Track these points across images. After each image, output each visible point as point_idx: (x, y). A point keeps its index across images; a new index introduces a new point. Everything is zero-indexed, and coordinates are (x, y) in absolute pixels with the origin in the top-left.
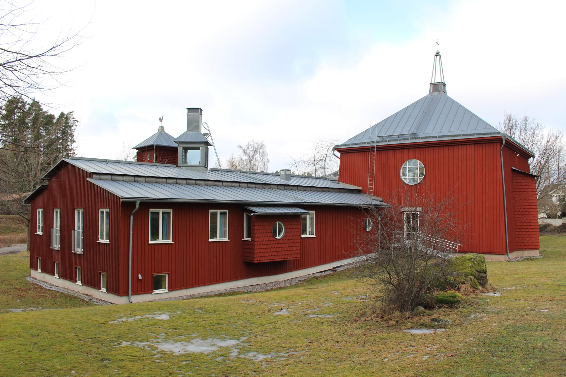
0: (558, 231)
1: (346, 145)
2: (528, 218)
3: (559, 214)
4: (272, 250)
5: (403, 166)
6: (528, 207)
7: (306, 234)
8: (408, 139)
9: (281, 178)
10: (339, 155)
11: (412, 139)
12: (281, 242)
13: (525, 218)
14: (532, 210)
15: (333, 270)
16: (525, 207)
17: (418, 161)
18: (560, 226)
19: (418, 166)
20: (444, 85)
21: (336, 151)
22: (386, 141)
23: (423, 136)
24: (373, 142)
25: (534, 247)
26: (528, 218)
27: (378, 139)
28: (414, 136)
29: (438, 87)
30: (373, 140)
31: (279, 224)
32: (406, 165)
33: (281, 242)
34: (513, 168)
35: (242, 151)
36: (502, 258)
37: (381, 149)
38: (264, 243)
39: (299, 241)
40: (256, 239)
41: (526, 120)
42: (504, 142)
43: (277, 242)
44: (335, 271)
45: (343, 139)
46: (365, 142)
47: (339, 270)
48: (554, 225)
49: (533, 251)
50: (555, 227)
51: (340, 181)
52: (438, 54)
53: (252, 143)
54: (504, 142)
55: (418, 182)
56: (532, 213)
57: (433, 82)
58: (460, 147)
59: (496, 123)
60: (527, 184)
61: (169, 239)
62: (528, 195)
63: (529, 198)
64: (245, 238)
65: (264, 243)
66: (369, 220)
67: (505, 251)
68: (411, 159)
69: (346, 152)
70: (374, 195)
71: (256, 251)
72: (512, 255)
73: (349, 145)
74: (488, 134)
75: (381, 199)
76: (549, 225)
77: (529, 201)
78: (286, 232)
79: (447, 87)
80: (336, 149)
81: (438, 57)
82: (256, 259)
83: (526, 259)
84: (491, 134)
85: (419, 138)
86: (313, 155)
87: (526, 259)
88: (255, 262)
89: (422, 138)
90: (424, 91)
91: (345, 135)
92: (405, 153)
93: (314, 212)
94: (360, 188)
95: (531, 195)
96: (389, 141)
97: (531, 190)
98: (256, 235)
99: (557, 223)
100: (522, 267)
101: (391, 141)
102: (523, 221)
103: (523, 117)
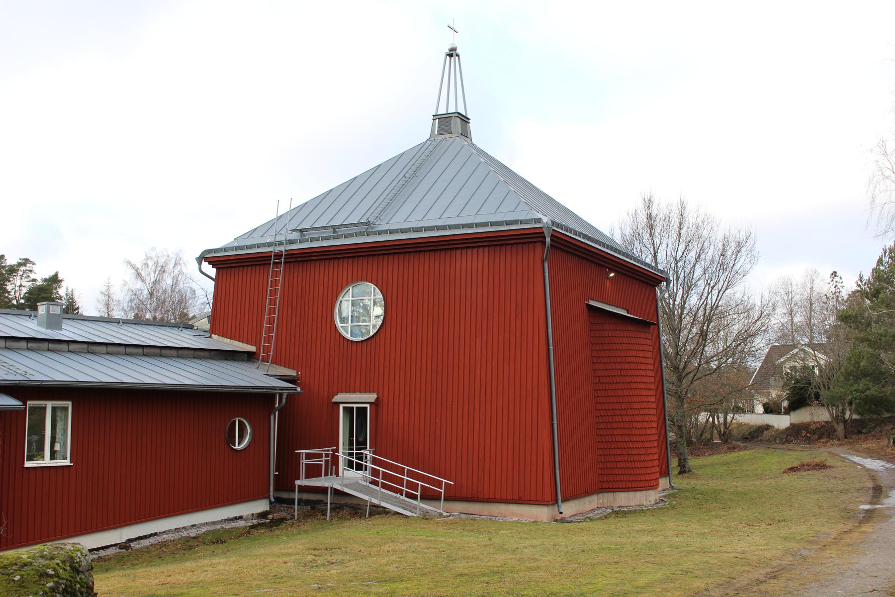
0: (781, 439)
1: (231, 249)
2: (627, 419)
3: (785, 404)
6: (626, 392)
7: (43, 457)
8: (351, 236)
9: (40, 324)
11: (361, 234)
13: (619, 419)
14: (635, 399)
15: (125, 546)
16: (620, 393)
17: (373, 286)
18: (787, 429)
20: (465, 120)
25: (647, 484)
26: (627, 419)
27: (295, 236)
28: (367, 226)
29: (452, 124)
30: (286, 239)
31: (240, 421)
34: (592, 303)
35: (131, 271)
36: (543, 513)
37: (298, 259)
41: (682, 205)
42: (548, 240)
45: (224, 236)
46: (267, 242)
48: (776, 426)
49: (638, 493)
50: (777, 430)
51: (213, 330)
53: (153, 254)
54: (548, 240)
55: (372, 334)
56: (636, 406)
57: (442, 111)
58: (459, 252)
59: (605, 213)
60: (625, 340)
62: (627, 366)
63: (630, 373)
67: (548, 496)
68: (357, 280)
69: (228, 265)
70: (275, 362)
72: (569, 509)
74: (515, 222)
75: (292, 373)
76: (768, 427)
77: (628, 379)
79: (472, 126)
80: (206, 259)
83: (619, 513)
84: (521, 222)
85: (380, 233)
87: (619, 513)
89: (385, 232)
90: (421, 131)
93: (69, 404)
94: (252, 349)
95: (633, 366)
96: (312, 240)
97: (634, 353)
99: (781, 422)
100: (594, 536)
101: (317, 239)
102: (614, 425)
103: (675, 202)
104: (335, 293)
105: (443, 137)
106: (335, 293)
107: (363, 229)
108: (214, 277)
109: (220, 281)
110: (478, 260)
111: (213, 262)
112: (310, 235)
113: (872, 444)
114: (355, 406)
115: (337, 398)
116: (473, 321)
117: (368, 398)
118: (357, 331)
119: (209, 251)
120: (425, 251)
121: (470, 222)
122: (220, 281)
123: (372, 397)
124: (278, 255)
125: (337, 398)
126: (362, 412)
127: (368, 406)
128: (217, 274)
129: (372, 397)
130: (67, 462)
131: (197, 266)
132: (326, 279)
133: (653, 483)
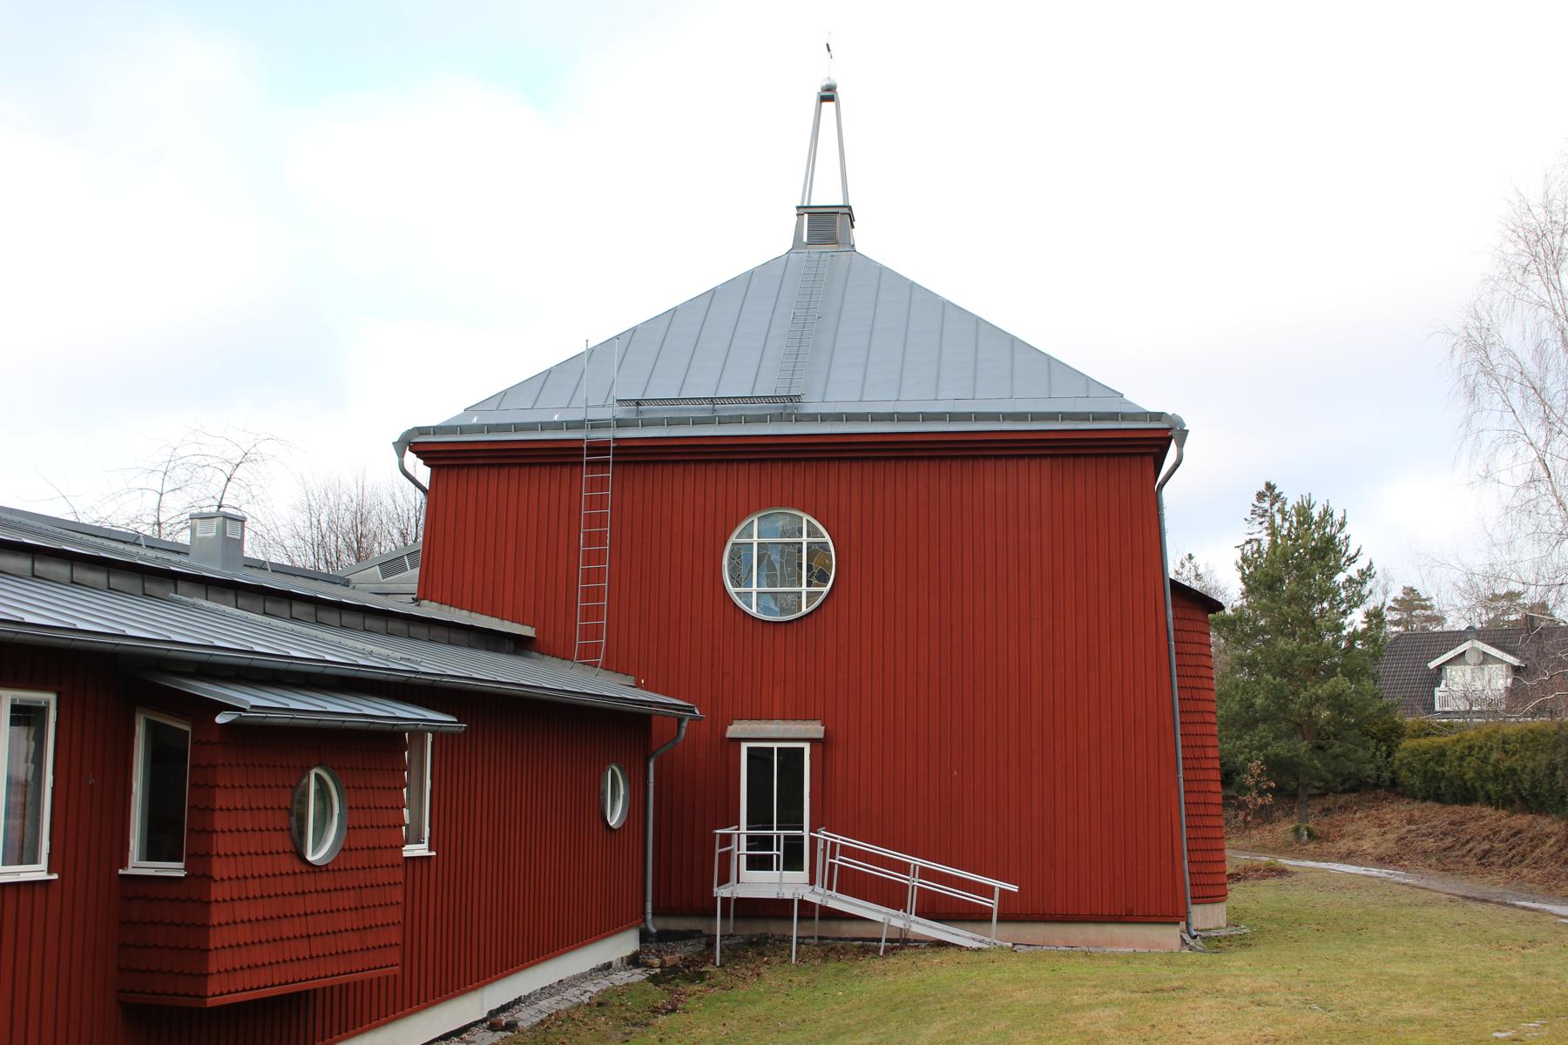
1: (463, 430)
4: (288, 929)
5: (733, 539)
8: (760, 419)
10: (423, 473)
12: (325, 881)
15: (492, 1022)
19: (805, 539)
21: (410, 458)
22: (658, 423)
24: (595, 425)
27: (621, 412)
28: (787, 406)
29: (826, 225)
30: (590, 409)
33: (325, 881)
38: (254, 887)
39: (399, 875)
40: (219, 868)
43: (309, 883)
44: (511, 1026)
45: (444, 404)
46: (557, 414)
47: (527, 1018)
49: (1209, 906)
55: (804, 610)
64: (137, 865)
65: (254, 887)
66: (613, 773)
69: (457, 462)
71: (216, 938)
73: (479, 429)
78: (349, 828)
81: (828, 107)
82: (213, 986)
85: (813, 418)
86: (151, 500)
88: (212, 1002)
90: (775, 235)
91: (458, 387)
94: (528, 631)
96: (672, 422)
98: (221, 844)
107: (774, 408)
108: (426, 484)
110: (1034, 478)
111: (427, 453)
112: (652, 412)
114: (775, 745)
115: (735, 730)
117: (801, 732)
120: (675, 462)
121: (1018, 410)
124: (598, 448)
125: (735, 730)
127: (807, 747)
128: (434, 479)
129: (816, 729)
130: (37, 872)
131: (396, 459)
133: (1218, 891)
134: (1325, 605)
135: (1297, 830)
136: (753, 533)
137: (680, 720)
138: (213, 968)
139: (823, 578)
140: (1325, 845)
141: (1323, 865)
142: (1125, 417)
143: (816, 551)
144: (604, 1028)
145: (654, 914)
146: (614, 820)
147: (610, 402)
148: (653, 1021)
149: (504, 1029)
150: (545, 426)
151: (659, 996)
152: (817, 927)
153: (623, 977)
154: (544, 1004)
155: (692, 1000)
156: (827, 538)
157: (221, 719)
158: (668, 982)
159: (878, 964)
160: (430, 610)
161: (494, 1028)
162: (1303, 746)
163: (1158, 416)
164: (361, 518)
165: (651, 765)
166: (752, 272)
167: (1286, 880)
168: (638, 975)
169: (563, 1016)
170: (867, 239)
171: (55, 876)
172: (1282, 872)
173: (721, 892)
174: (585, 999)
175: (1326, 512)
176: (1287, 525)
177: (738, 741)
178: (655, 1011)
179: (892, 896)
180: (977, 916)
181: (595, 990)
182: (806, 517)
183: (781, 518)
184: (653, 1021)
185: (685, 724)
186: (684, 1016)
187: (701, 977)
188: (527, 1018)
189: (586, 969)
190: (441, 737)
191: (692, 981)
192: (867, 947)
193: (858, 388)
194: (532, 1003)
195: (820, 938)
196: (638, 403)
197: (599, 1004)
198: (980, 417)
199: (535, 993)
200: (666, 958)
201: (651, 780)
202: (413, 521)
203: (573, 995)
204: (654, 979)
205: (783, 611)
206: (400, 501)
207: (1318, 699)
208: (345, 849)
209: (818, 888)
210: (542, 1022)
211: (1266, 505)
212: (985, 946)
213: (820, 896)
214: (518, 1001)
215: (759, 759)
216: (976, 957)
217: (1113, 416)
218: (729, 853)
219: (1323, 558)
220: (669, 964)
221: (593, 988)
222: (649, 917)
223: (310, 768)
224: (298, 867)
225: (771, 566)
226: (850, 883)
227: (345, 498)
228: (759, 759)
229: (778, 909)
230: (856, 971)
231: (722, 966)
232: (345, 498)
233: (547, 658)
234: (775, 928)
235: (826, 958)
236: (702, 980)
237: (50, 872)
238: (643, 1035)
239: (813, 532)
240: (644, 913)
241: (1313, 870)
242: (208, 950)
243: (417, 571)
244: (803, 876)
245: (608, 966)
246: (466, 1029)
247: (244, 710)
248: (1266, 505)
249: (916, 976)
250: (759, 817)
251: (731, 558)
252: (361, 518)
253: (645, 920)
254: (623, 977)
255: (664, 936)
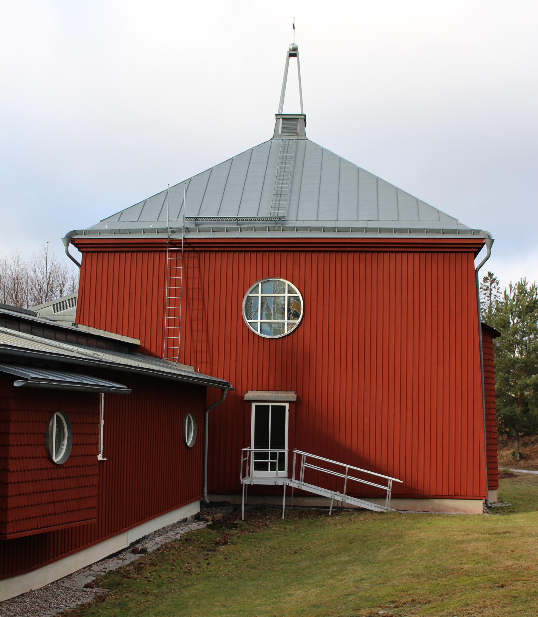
5: (248, 294)
10: (78, 256)
15: (133, 548)
21: (71, 247)
22: (207, 230)
23: (299, 224)
28: (278, 221)
29: (291, 124)
32: (255, 290)
45: (90, 219)
47: (151, 546)
49: (493, 491)
52: (293, 53)
55: (286, 332)
61: (285, 407)
69: (92, 248)
81: (293, 60)
85: (292, 229)
88: (9, 537)
90: (265, 130)
92: (253, 261)
94: (137, 342)
101: (221, 230)
104: (241, 287)
105: (286, 138)
106: (241, 287)
109: (88, 267)
110: (411, 263)
111: (80, 245)
113: (50, 446)
114: (270, 404)
115: (250, 395)
116: (404, 323)
118: (267, 328)
119: (75, 232)
122: (88, 267)
123: (292, 396)
124: (174, 243)
126: (279, 411)
127: (287, 405)
129: (292, 396)
131: (64, 248)
132: (230, 272)
134: (532, 336)
135: (514, 454)
136: (259, 293)
137: (223, 390)
138: (10, 519)
139: (296, 316)
140: (529, 462)
141: (530, 472)
142: (459, 232)
143: (293, 302)
144: (192, 552)
145: (208, 493)
146: (189, 443)
147: (181, 218)
148: (217, 549)
149: (140, 552)
150: (145, 231)
151: (215, 535)
152: (294, 500)
153: (195, 526)
154: (158, 539)
155: (234, 538)
156: (299, 294)
157: (16, 384)
158: (218, 528)
159: (329, 519)
160: (83, 328)
161: (135, 552)
162: (518, 410)
163: (478, 232)
164: (17, 280)
165: (207, 414)
166: (252, 150)
167: (514, 479)
168: (201, 525)
169: (169, 546)
170: (312, 132)
171: (105, 459)
172: (512, 475)
173: (246, 481)
174: (178, 537)
175: (533, 287)
176: (513, 294)
177: (250, 402)
178: (217, 543)
179: (334, 484)
180: (379, 495)
181: (183, 532)
182: (287, 282)
183: (8, 304)
184: (217, 549)
185: (226, 392)
186: (233, 546)
187: (235, 526)
188: (151, 546)
189: (175, 521)
190: (111, 396)
191: (231, 528)
192: (321, 511)
193: (315, 215)
194: (151, 540)
195: (294, 506)
196: (196, 219)
197: (186, 540)
198: (381, 230)
199: (152, 534)
200: (215, 516)
201: (207, 422)
202: (45, 284)
203: (171, 535)
204: (209, 527)
205: (275, 332)
206: (38, 273)
207: (528, 386)
208: (71, 456)
209: (293, 480)
210: (159, 549)
211: (488, 284)
212: (385, 511)
213: (294, 484)
214: (144, 538)
215: (262, 411)
216: (382, 517)
217: (454, 231)
218: (246, 460)
219: (531, 312)
220: (216, 519)
221: (182, 531)
222: (206, 494)
223: (54, 412)
224: (49, 465)
225: (268, 309)
226: (311, 477)
227: (8, 271)
228: (262, 411)
229: (275, 490)
230: (319, 523)
231: (245, 520)
232: (8, 271)
233: (150, 357)
234: (270, 501)
235: (300, 517)
236: (236, 528)
237: (103, 457)
238: (215, 556)
239: (290, 291)
240: (203, 492)
241: (527, 474)
242: (7, 509)
243: (75, 308)
244: (284, 473)
245: (185, 520)
246: (120, 552)
247: (27, 379)
248: (488, 284)
249: (353, 526)
250: (261, 442)
251: (246, 304)
252: (17, 280)
253: (203, 496)
254: (195, 526)
255: (212, 504)
